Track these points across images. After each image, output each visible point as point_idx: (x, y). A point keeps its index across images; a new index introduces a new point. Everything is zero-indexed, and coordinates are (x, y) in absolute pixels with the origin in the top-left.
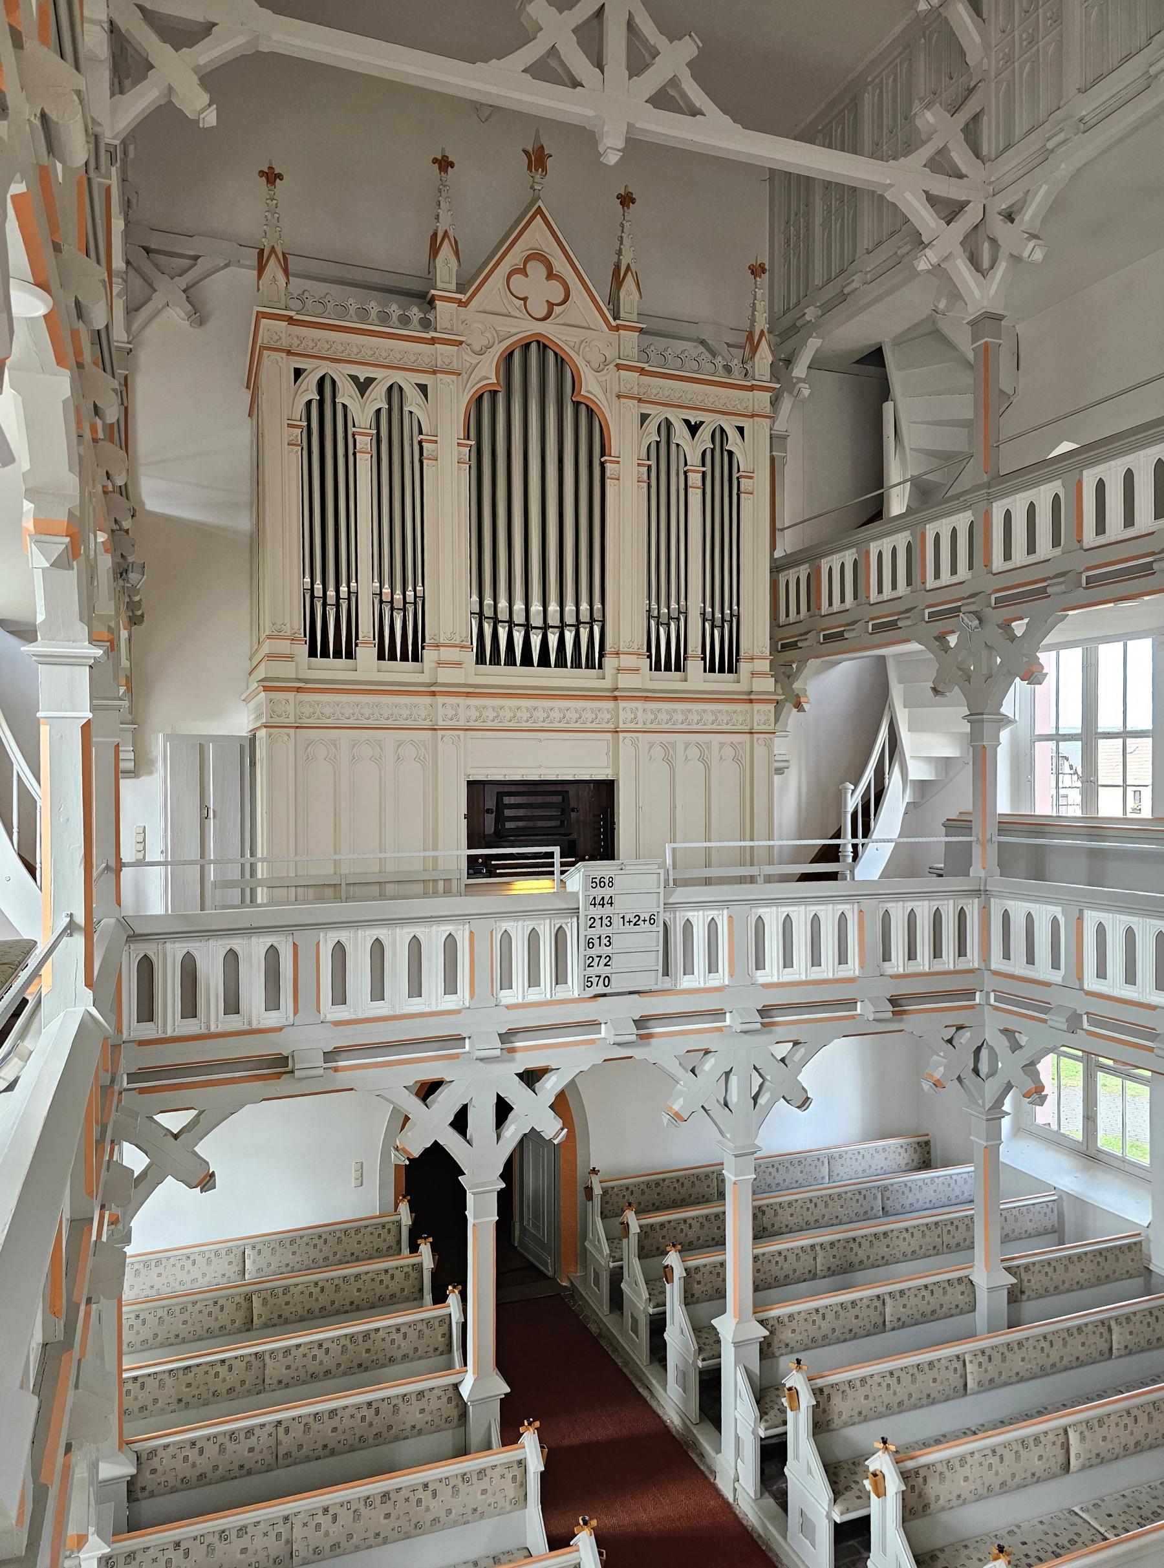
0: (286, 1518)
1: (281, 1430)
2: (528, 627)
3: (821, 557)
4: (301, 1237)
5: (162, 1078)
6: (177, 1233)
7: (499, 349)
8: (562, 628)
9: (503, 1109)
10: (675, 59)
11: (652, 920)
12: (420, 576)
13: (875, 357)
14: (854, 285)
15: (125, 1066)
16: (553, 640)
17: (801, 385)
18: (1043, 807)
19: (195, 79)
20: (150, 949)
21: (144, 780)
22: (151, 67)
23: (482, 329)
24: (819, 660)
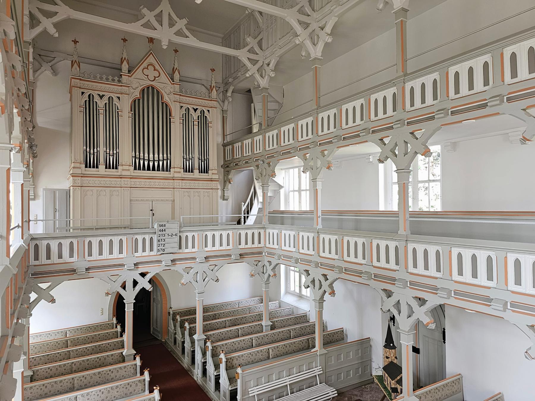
0: (73, 379)
1: (73, 365)
2: (149, 161)
5: (41, 274)
6: (45, 322)
8: (159, 161)
9: (135, 283)
10: (181, 24)
11: (176, 235)
12: (117, 147)
13: (249, 91)
15: (31, 271)
16: (156, 164)
18: (291, 209)
20: (37, 242)
21: (36, 202)
22: (41, 23)
23: (136, 82)
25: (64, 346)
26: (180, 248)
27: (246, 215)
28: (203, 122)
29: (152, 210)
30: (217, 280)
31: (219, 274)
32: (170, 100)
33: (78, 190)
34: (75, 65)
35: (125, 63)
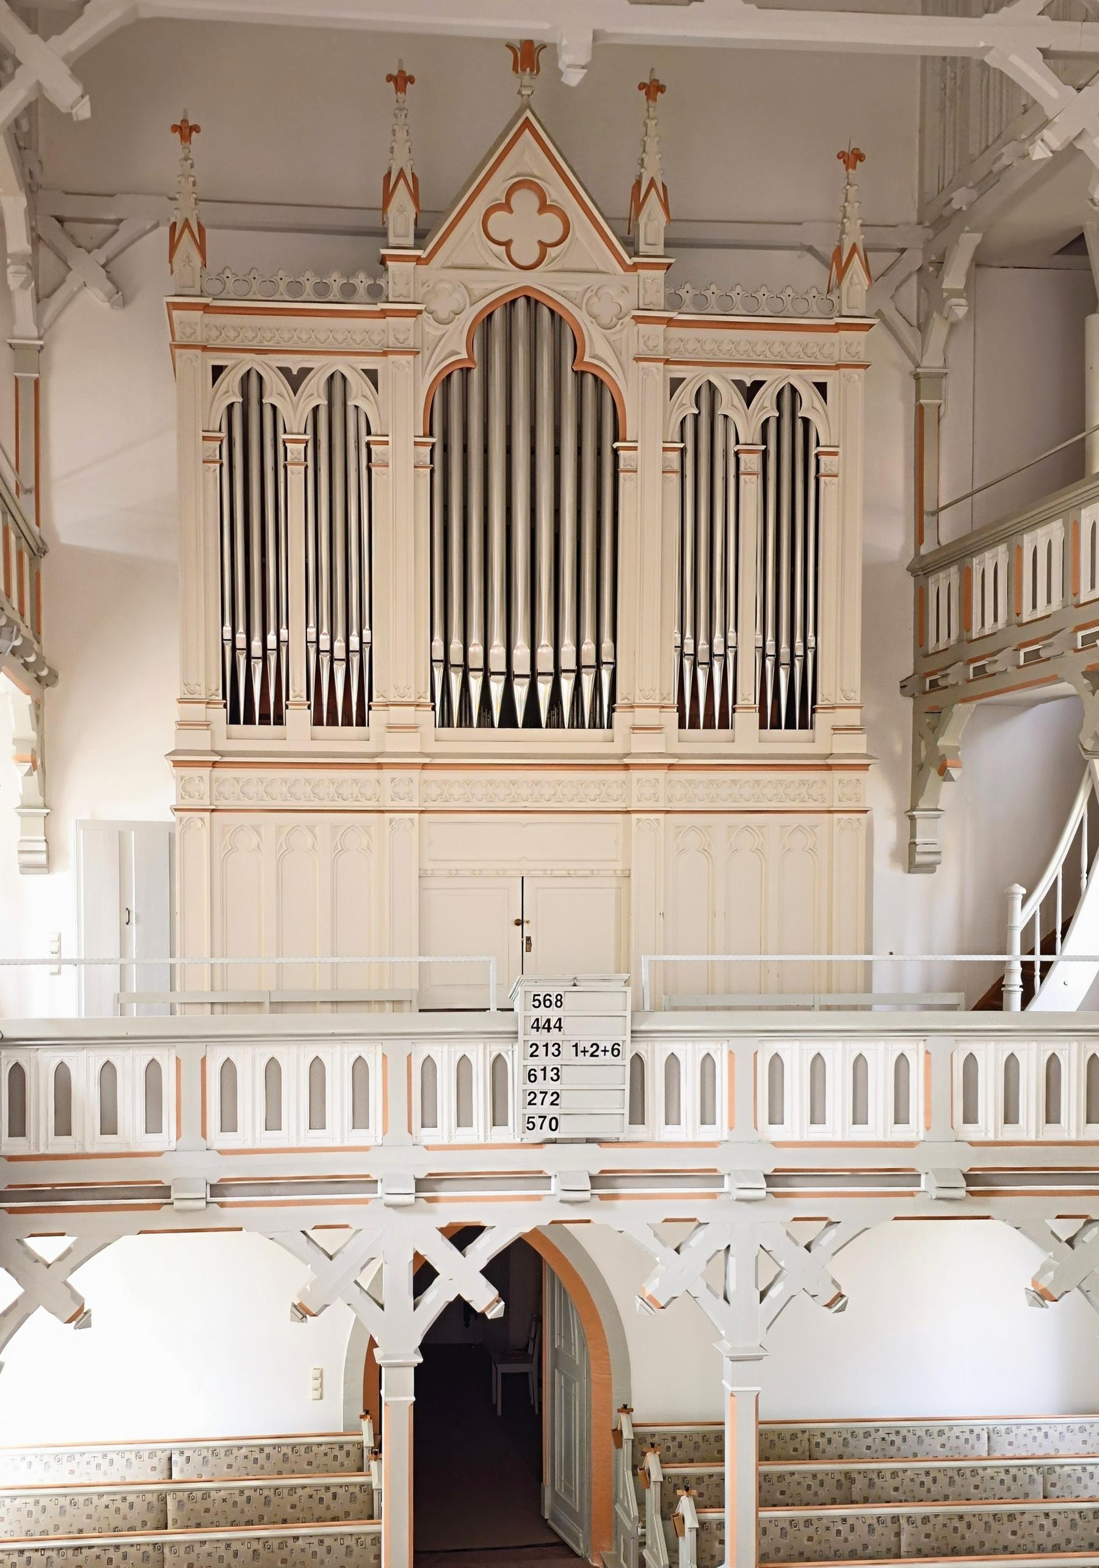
2: (509, 676)
3: (972, 554)
4: (240, 1448)
7: (471, 313)
8: (533, 676)
9: (424, 1276)
11: (615, 1050)
12: (366, 619)
14: (1005, 161)
16: (544, 690)
17: (954, 301)
19: (65, 70)
23: (449, 293)
24: (973, 705)
25: (151, 1518)
26: (637, 1115)
27: (1038, 958)
28: (793, 453)
29: (519, 923)
30: (837, 1303)
31: (847, 1271)
32: (618, 356)
33: (201, 823)
34: (186, 243)
35: (401, 195)
